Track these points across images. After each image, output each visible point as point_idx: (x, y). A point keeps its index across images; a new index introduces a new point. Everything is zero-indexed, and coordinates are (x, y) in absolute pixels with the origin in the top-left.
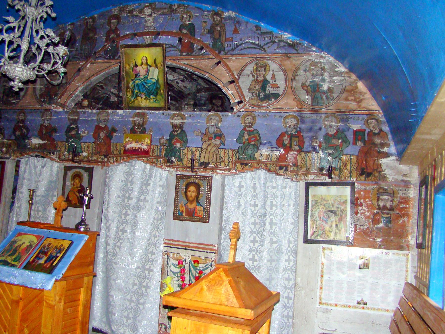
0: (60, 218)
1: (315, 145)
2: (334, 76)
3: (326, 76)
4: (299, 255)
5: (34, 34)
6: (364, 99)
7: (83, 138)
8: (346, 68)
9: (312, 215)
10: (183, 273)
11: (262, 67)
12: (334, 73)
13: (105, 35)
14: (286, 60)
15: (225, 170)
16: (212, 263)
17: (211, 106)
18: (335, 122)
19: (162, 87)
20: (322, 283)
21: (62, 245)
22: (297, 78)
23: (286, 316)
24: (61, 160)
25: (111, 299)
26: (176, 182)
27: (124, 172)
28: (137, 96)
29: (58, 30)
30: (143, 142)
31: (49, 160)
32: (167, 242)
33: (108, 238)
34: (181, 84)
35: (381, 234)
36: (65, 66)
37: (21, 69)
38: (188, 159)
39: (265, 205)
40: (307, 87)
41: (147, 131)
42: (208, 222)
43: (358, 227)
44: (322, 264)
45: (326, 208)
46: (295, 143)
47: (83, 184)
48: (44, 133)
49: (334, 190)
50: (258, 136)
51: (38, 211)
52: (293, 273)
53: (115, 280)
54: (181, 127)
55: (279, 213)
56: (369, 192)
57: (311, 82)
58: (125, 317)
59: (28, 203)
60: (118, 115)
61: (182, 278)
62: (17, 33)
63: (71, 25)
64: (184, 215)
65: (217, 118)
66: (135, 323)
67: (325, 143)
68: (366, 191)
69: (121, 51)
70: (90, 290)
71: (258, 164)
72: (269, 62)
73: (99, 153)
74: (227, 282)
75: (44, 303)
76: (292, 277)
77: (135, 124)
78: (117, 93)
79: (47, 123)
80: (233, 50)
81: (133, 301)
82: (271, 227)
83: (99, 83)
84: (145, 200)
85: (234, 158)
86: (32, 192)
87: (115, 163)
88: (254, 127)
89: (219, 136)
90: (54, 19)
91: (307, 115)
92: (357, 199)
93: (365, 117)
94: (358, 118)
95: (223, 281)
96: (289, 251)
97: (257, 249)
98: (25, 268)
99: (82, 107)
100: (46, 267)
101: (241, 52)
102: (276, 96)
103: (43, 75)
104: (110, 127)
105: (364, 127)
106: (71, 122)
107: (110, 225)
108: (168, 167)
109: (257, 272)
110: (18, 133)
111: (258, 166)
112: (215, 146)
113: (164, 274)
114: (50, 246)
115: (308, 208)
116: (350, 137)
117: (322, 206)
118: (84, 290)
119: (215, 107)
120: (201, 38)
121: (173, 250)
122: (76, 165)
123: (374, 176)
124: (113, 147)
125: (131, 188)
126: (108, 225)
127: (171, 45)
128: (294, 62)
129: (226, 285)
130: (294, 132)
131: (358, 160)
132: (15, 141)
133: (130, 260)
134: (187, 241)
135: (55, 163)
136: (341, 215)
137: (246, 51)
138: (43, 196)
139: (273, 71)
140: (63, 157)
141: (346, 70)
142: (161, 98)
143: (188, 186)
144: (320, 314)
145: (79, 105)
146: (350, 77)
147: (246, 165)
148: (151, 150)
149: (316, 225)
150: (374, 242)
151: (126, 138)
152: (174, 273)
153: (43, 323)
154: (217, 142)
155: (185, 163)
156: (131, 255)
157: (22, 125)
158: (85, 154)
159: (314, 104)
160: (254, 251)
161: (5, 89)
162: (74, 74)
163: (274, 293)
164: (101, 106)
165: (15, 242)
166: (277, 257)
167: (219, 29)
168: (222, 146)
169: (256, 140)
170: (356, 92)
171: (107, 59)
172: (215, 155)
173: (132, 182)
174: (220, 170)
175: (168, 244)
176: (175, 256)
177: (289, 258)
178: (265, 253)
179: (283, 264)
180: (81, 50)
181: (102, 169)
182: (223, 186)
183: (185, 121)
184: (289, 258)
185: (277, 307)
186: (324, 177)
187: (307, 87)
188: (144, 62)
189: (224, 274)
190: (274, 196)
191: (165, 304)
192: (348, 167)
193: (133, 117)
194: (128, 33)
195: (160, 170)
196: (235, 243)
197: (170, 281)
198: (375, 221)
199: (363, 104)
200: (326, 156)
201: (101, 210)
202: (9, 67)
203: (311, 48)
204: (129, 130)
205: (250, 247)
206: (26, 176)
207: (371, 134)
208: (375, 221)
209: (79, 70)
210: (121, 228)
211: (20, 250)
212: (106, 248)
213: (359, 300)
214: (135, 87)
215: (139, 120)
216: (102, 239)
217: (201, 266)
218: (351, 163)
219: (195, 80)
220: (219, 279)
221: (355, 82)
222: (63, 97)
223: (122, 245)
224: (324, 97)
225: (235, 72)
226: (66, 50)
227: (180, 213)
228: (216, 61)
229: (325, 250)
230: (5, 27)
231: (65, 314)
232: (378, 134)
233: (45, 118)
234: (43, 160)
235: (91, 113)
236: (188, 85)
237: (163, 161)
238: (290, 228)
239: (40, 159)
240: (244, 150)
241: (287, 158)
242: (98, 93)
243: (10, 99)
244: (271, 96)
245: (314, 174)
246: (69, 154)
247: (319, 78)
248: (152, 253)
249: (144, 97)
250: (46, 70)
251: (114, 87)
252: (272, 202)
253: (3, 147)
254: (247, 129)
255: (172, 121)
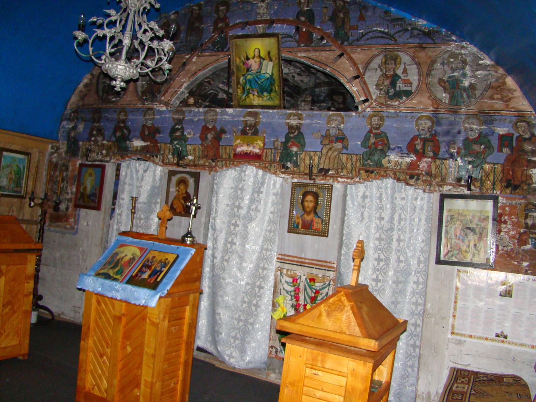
0: (164, 228)
1: (452, 151)
2: (477, 70)
3: (468, 70)
4: (429, 277)
5: (137, 27)
6: (514, 98)
7: (189, 140)
8: (492, 60)
9: (447, 232)
10: (297, 292)
11: (392, 60)
12: (478, 67)
13: (212, 24)
14: (420, 51)
15: (347, 178)
16: (330, 283)
17: (330, 103)
18: (476, 125)
19: (277, 83)
20: (455, 310)
21: (167, 259)
22: (433, 73)
23: (412, 346)
24: (164, 164)
25: (217, 317)
26: (292, 190)
27: (234, 178)
28: (249, 93)
29: (161, 19)
30: (255, 145)
31: (152, 164)
32: (280, 256)
33: (215, 251)
34: (297, 78)
35: (528, 257)
36: (170, 62)
37: (123, 67)
38: (305, 165)
39: (392, 218)
40: (445, 83)
41: (260, 132)
42: (327, 236)
43: (500, 248)
44: (457, 288)
45: (464, 225)
46: (429, 148)
47: (188, 191)
48: (146, 134)
49: (473, 204)
50: (385, 140)
51: (140, 219)
52: (422, 297)
53: (222, 297)
54: (298, 128)
55: (407, 228)
56: (515, 207)
57: (450, 77)
58: (233, 337)
59: (130, 212)
60: (227, 114)
61: (296, 297)
62: (119, 27)
63: (174, 14)
64: (300, 227)
65: (339, 118)
66: (243, 344)
67: (465, 149)
68: (511, 206)
69: (231, 42)
70: (196, 308)
71: (385, 171)
72: (400, 54)
73: (207, 156)
74: (349, 308)
75: (148, 321)
76: (420, 301)
77: (246, 125)
78: (226, 89)
79: (149, 123)
80: (358, 40)
81: (241, 320)
82: (399, 244)
83: (206, 78)
84: (257, 210)
85: (358, 165)
86: (134, 200)
87: (224, 168)
88: (382, 129)
89: (342, 139)
90: (157, 10)
91: (444, 116)
92: (501, 215)
93: (514, 119)
94: (505, 120)
95: (345, 306)
96: (418, 272)
97: (381, 268)
98: (128, 282)
99: (188, 105)
100: (150, 283)
101: (368, 42)
102: (408, 94)
103: (147, 73)
104: (218, 128)
105: (512, 131)
106: (176, 121)
107: (217, 236)
108: (283, 173)
109: (381, 295)
110: (118, 134)
111: (385, 175)
112: (336, 150)
113: (275, 293)
114: (154, 260)
115: (442, 224)
116: (495, 142)
117: (459, 223)
118: (190, 309)
119: (336, 104)
120: (321, 26)
121: (286, 266)
122: (181, 169)
123: (523, 189)
124: (222, 150)
125: (241, 196)
126: (215, 236)
127: (286, 34)
128: (430, 54)
129: (347, 311)
130: (428, 136)
131: (503, 169)
132: (116, 144)
133: (239, 275)
134: (303, 256)
135: (158, 166)
136: (481, 234)
137: (373, 42)
138: (145, 203)
139: (405, 64)
140: (167, 161)
141: (492, 63)
142: (275, 95)
143: (305, 195)
144: (451, 346)
145: (184, 103)
146: (496, 72)
147: (372, 172)
148: (264, 154)
149: (451, 244)
150: (520, 266)
151: (236, 140)
152: (287, 292)
153: (146, 342)
154: (339, 145)
155: (302, 169)
156: (239, 270)
157: (122, 125)
158: (190, 158)
159: (452, 103)
160: (378, 270)
161: (104, 86)
162: (179, 68)
163: (401, 321)
164: (208, 104)
165: (116, 254)
166: (404, 278)
167: (341, 15)
168: (344, 151)
169: (383, 144)
170: (504, 89)
171: (215, 51)
172: (336, 160)
173: (242, 189)
174: (342, 178)
175: (281, 259)
176: (289, 273)
177: (418, 279)
178: (391, 273)
179: (410, 287)
180: (186, 42)
181: (210, 174)
182: (345, 196)
183: (303, 122)
184: (418, 279)
185: (403, 337)
186: (462, 188)
187: (445, 83)
188: (257, 54)
189: (345, 298)
190: (403, 209)
191: (278, 328)
192: (491, 178)
193: (244, 117)
194: (238, 21)
195: (273, 177)
196: (358, 264)
197: (282, 301)
198: (522, 242)
199: (512, 104)
200: (465, 164)
201: (207, 219)
202: (110, 66)
203: (450, 37)
204: (240, 132)
205: (374, 265)
206: (127, 181)
207: (520, 139)
208: (522, 242)
209: (184, 64)
210: (230, 240)
211: (123, 262)
212: (213, 261)
213: (499, 332)
214: (246, 83)
215: (250, 120)
216: (209, 253)
217: (318, 285)
218: (494, 173)
219: (313, 74)
220: (340, 304)
221: (503, 77)
222: (167, 95)
223: (231, 259)
224: (465, 95)
225: (360, 66)
226: (172, 45)
227: (295, 225)
228: (338, 52)
229: (460, 273)
230: (106, 22)
231: (169, 333)
232: (529, 139)
233: (147, 117)
234: (145, 163)
235: (197, 112)
236: (306, 80)
237: (277, 166)
238: (419, 245)
239: (142, 162)
240: (370, 155)
241: (419, 166)
242: (205, 89)
243: (110, 97)
244: (402, 93)
245: (450, 184)
246: (174, 157)
247: (458, 72)
248: (264, 269)
249: (256, 94)
250: (149, 68)
251: (223, 83)
252: (400, 216)
253: (103, 150)
254: (374, 131)
255: (287, 121)
